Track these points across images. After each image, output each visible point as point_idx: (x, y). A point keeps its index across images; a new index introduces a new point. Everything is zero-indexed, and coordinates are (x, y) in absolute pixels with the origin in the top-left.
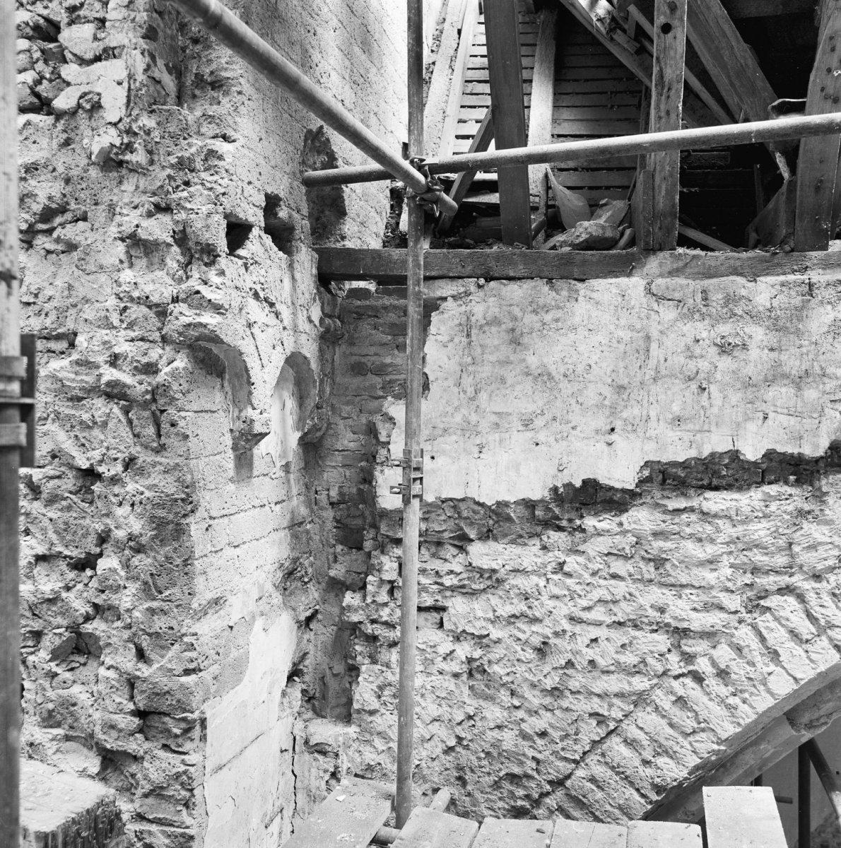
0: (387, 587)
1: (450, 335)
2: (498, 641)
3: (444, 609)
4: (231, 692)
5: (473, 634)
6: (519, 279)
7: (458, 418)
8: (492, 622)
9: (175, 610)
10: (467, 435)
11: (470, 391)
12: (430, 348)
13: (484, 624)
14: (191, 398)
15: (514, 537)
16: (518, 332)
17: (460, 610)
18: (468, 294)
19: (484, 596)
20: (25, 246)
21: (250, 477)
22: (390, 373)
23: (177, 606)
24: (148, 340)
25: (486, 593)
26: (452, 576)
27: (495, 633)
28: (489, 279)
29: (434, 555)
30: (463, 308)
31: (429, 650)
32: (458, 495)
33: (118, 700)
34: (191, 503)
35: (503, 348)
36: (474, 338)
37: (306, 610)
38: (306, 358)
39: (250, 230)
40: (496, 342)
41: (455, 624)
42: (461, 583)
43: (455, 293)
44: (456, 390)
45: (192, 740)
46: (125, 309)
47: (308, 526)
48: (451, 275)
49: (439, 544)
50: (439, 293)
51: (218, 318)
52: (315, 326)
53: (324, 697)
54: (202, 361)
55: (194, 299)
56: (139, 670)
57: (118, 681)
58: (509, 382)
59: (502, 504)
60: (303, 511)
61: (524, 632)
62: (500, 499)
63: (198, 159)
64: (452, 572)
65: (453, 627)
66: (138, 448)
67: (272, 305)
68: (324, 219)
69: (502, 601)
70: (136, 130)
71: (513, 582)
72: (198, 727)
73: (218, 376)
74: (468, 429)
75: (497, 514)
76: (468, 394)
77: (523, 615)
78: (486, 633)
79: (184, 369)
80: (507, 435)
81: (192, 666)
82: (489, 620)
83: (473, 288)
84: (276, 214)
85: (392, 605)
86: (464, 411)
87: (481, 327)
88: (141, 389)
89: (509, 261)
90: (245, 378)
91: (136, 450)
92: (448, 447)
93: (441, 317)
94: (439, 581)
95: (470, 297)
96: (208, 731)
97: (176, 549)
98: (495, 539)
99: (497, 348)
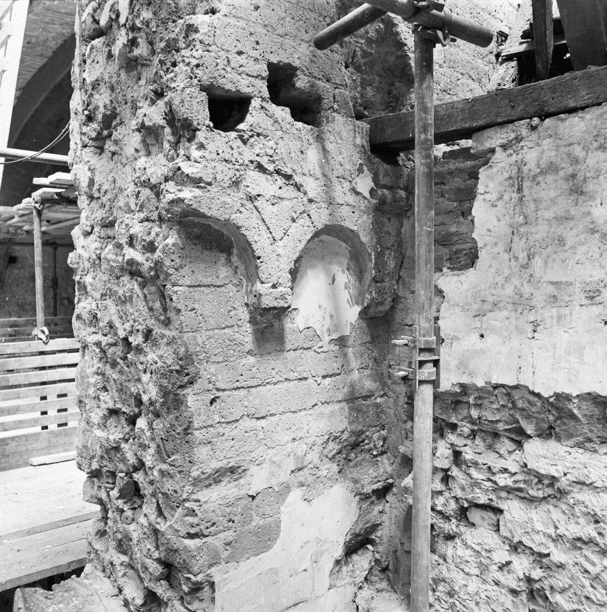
0: (440, 475)
1: (499, 192)
2: (561, 566)
3: (501, 511)
4: (252, 558)
5: (531, 549)
6: (583, 108)
7: (509, 290)
8: (554, 540)
9: (178, 475)
10: (520, 310)
11: (522, 256)
12: (479, 210)
13: (544, 540)
14: (184, 273)
15: (581, 439)
16: (580, 177)
17: (517, 517)
18: (519, 139)
19: (544, 507)
20: (99, 151)
21: (282, 350)
22: (456, 243)
23: (180, 472)
24: (151, 220)
25: (548, 503)
26: (506, 475)
27: (558, 555)
28: (543, 116)
29: (490, 447)
30: (514, 158)
31: (483, 553)
32: (511, 382)
33: (149, 546)
34: (187, 374)
35: (561, 200)
36: (526, 192)
37: (372, 483)
38: (352, 231)
39: (250, 103)
40: (553, 194)
41: (511, 532)
42: (517, 486)
43: (505, 141)
44: (506, 256)
45: (201, 600)
46: (139, 192)
47: (379, 400)
48: (500, 120)
49: (496, 435)
50: (488, 145)
51: (197, 192)
52: (364, 197)
53: (396, 571)
54: (198, 237)
55: (177, 176)
56: (158, 523)
57: (148, 529)
58: (569, 243)
59: (562, 397)
60: (369, 385)
61: (594, 564)
62: (559, 391)
63: (181, 38)
64: (505, 470)
65: (508, 535)
66: (153, 321)
67: (288, 177)
68: (395, 92)
69: (566, 517)
70: (139, 26)
71: (579, 497)
72: (207, 588)
73: (222, 251)
74: (521, 303)
75: (557, 409)
76: (521, 260)
77: (590, 542)
78: (546, 552)
79: (173, 245)
80: (566, 311)
81: (192, 531)
82: (550, 536)
83: (524, 132)
84: (294, 85)
85: (447, 494)
86: (516, 281)
87: (535, 177)
88: (147, 265)
89: (571, 90)
90: (250, 252)
91: (151, 323)
92: (497, 324)
93: (489, 172)
94: (492, 478)
95: (522, 144)
96: (216, 595)
97: (177, 417)
98: (559, 439)
99: (553, 201)
